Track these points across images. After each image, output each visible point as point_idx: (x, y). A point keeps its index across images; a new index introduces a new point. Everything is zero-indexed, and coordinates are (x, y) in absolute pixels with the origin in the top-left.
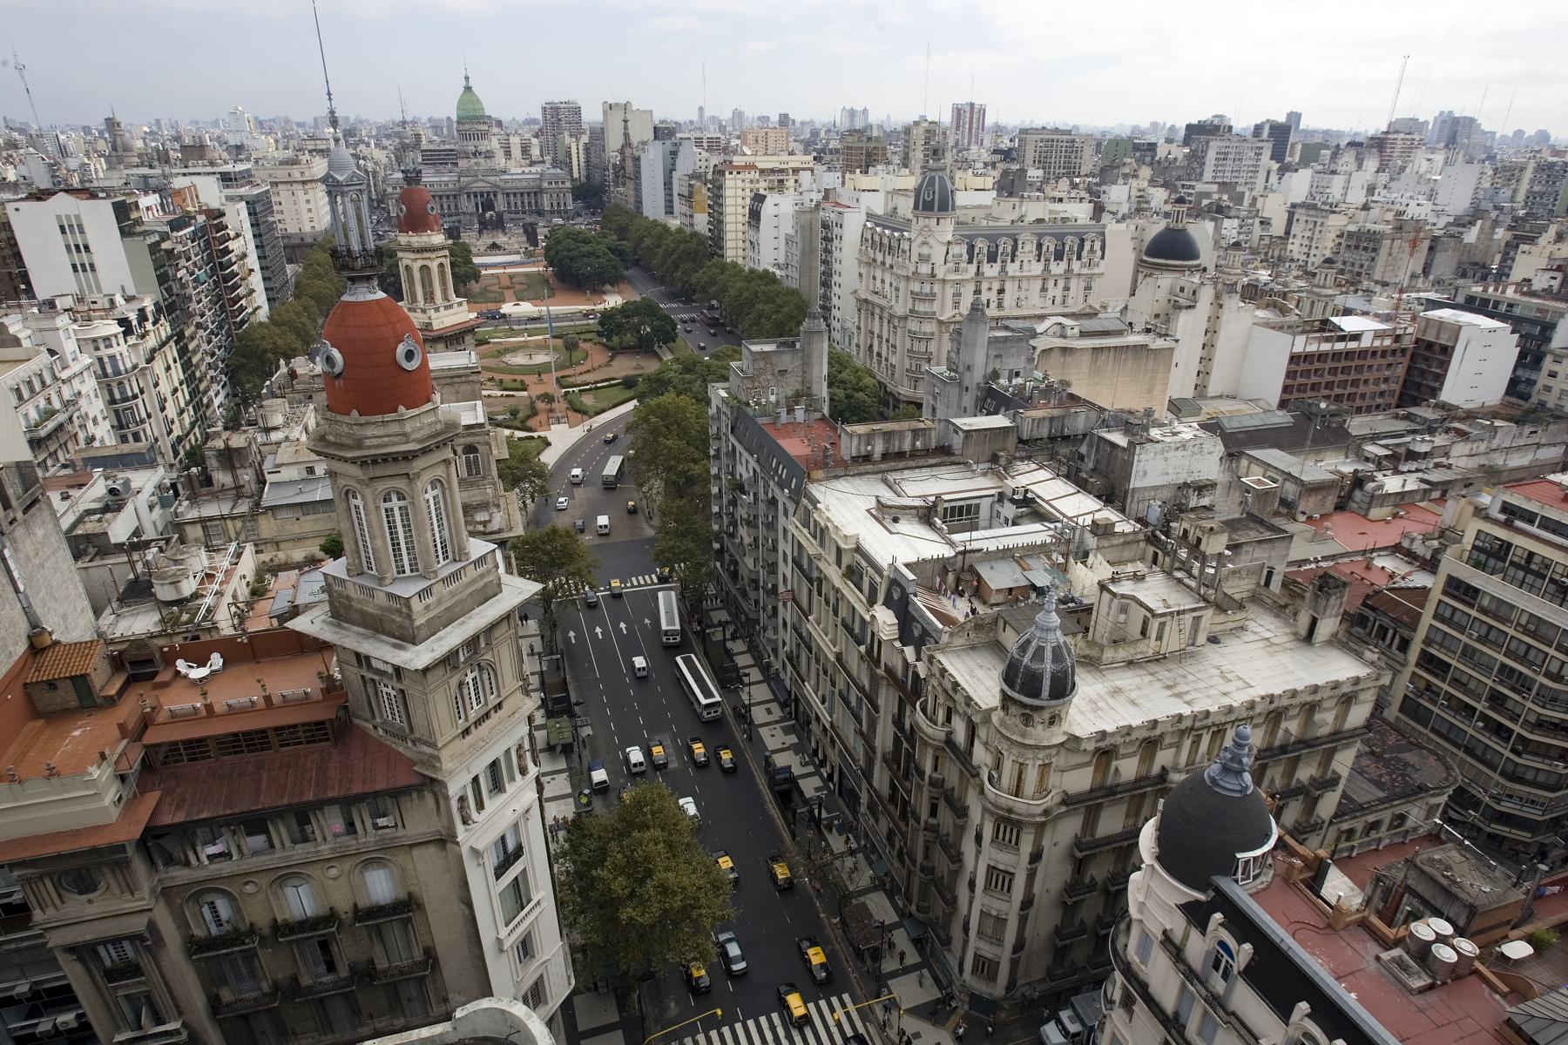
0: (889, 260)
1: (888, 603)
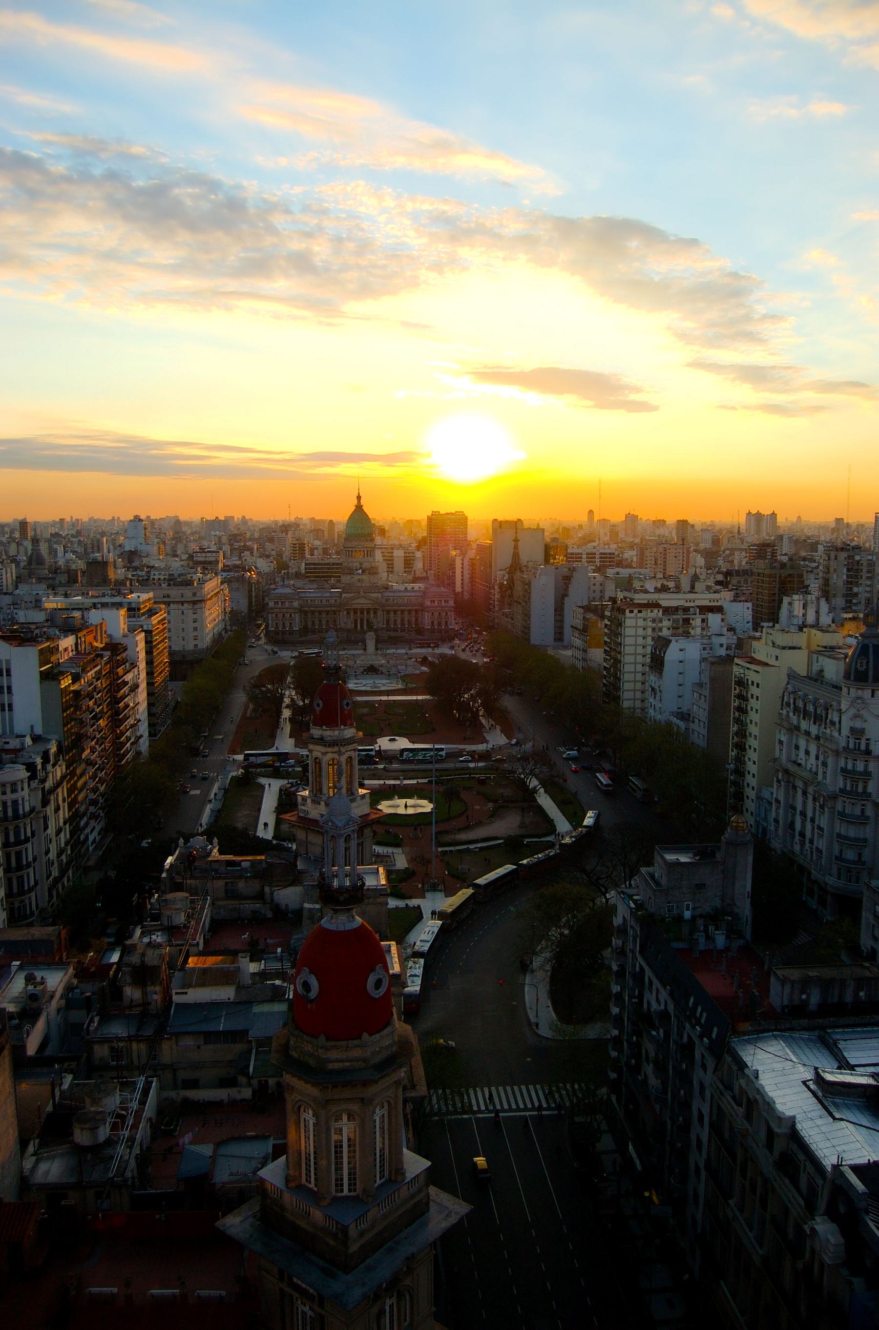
1: (832, 1214)
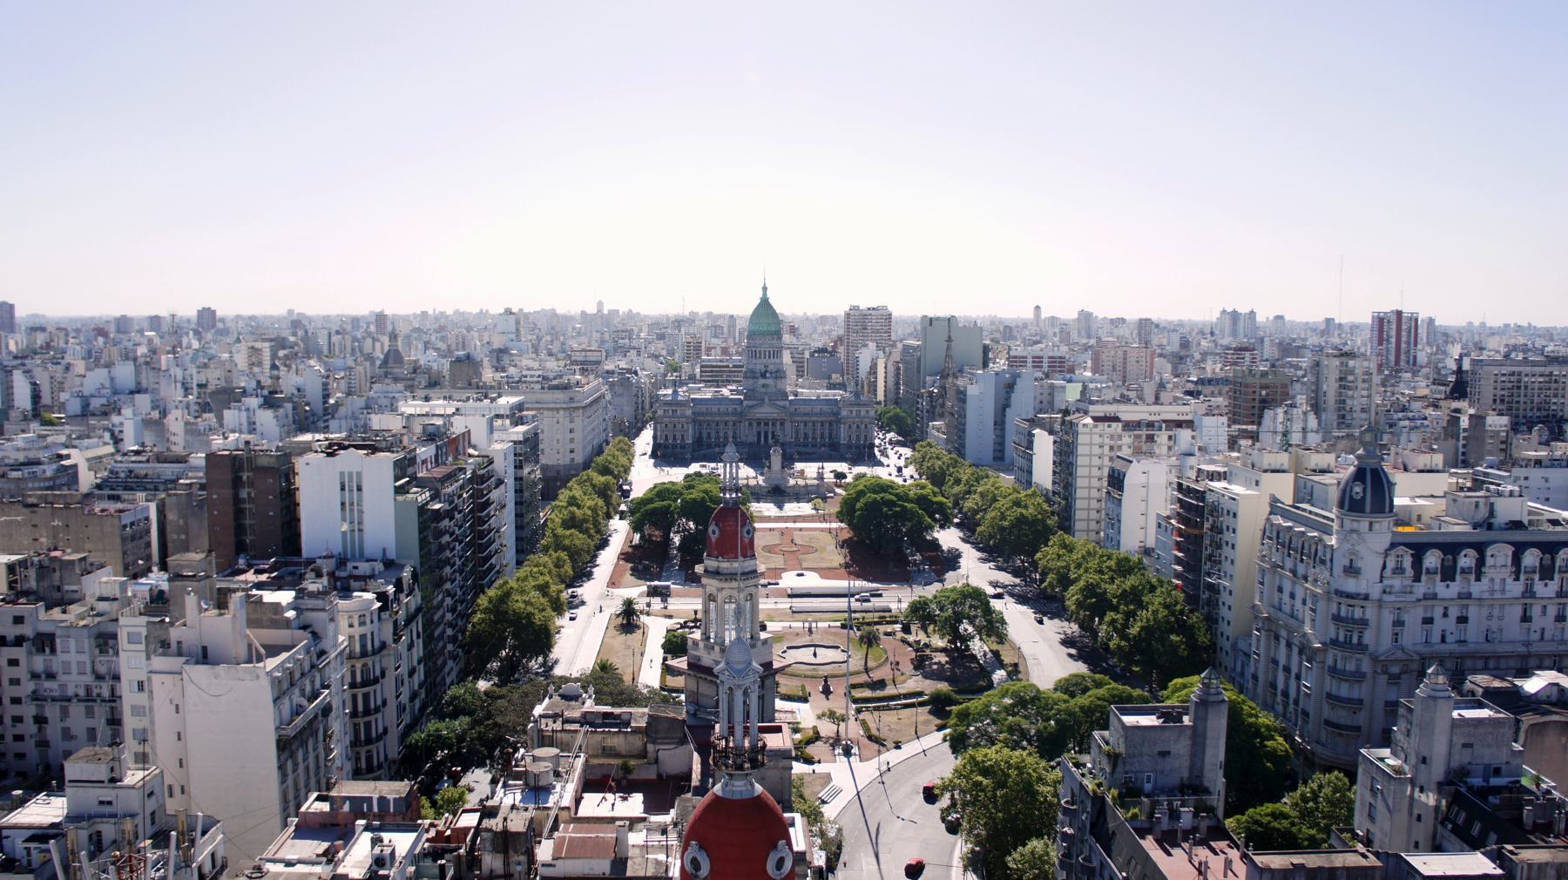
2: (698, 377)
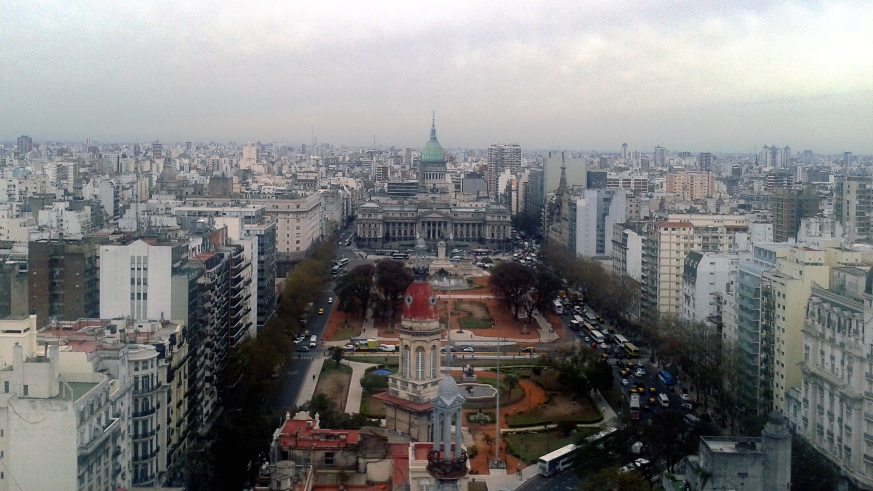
0: (839, 338)
2: (386, 190)
